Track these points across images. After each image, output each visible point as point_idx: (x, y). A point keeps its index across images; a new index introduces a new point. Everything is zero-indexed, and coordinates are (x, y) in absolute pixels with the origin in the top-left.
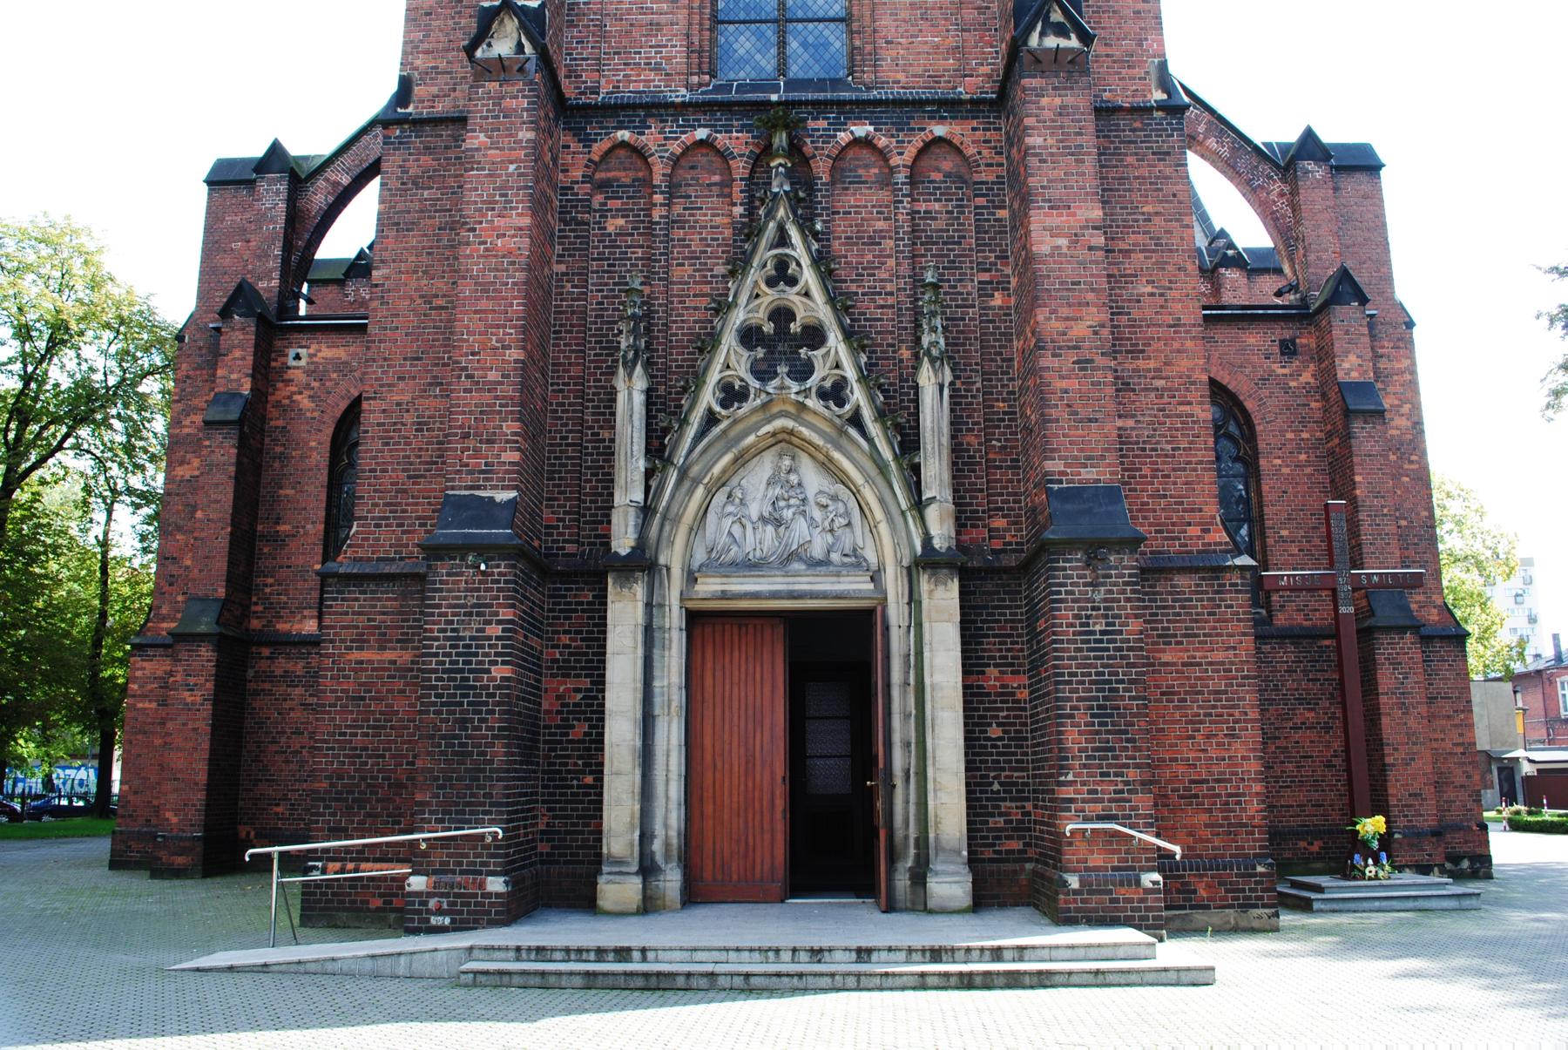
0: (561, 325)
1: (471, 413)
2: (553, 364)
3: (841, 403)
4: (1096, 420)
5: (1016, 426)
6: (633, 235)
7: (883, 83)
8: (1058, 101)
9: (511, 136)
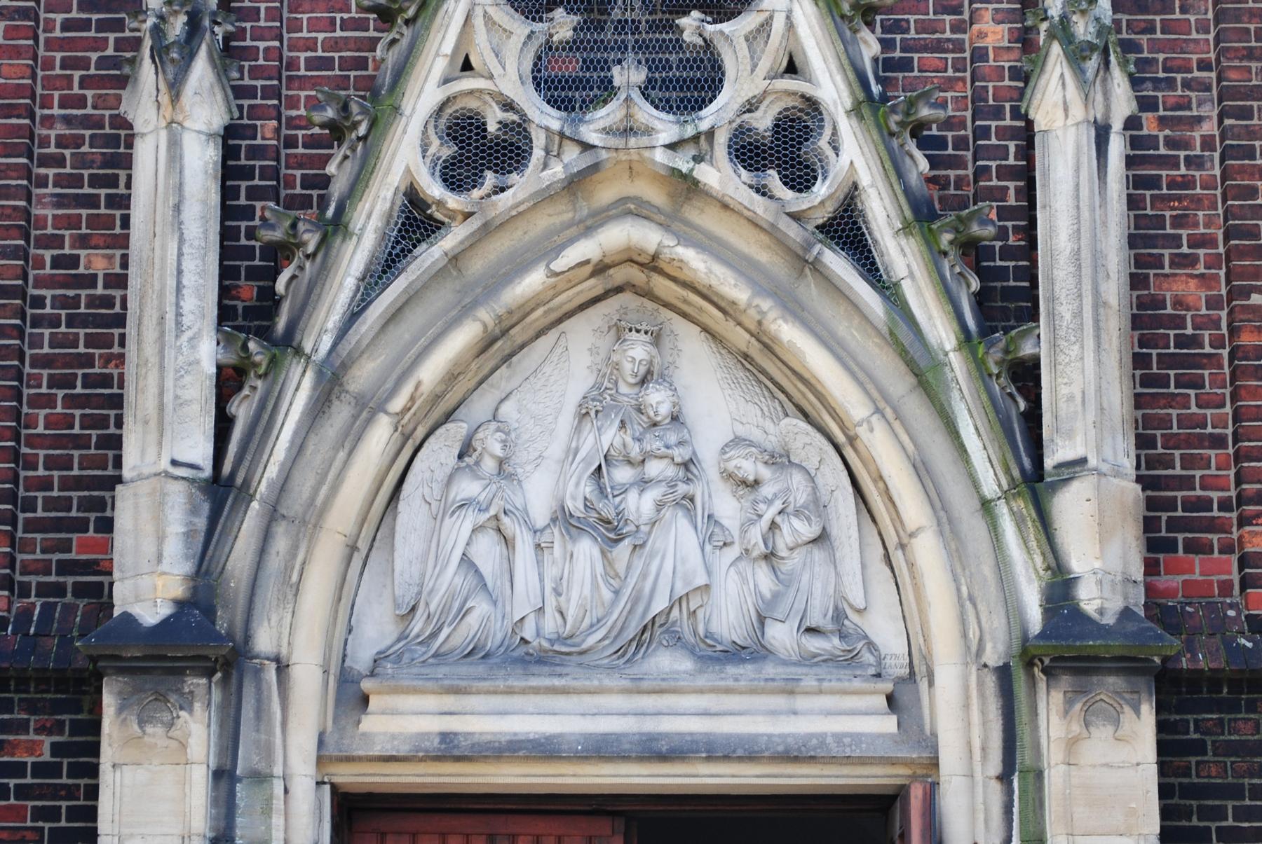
3: (801, 179)
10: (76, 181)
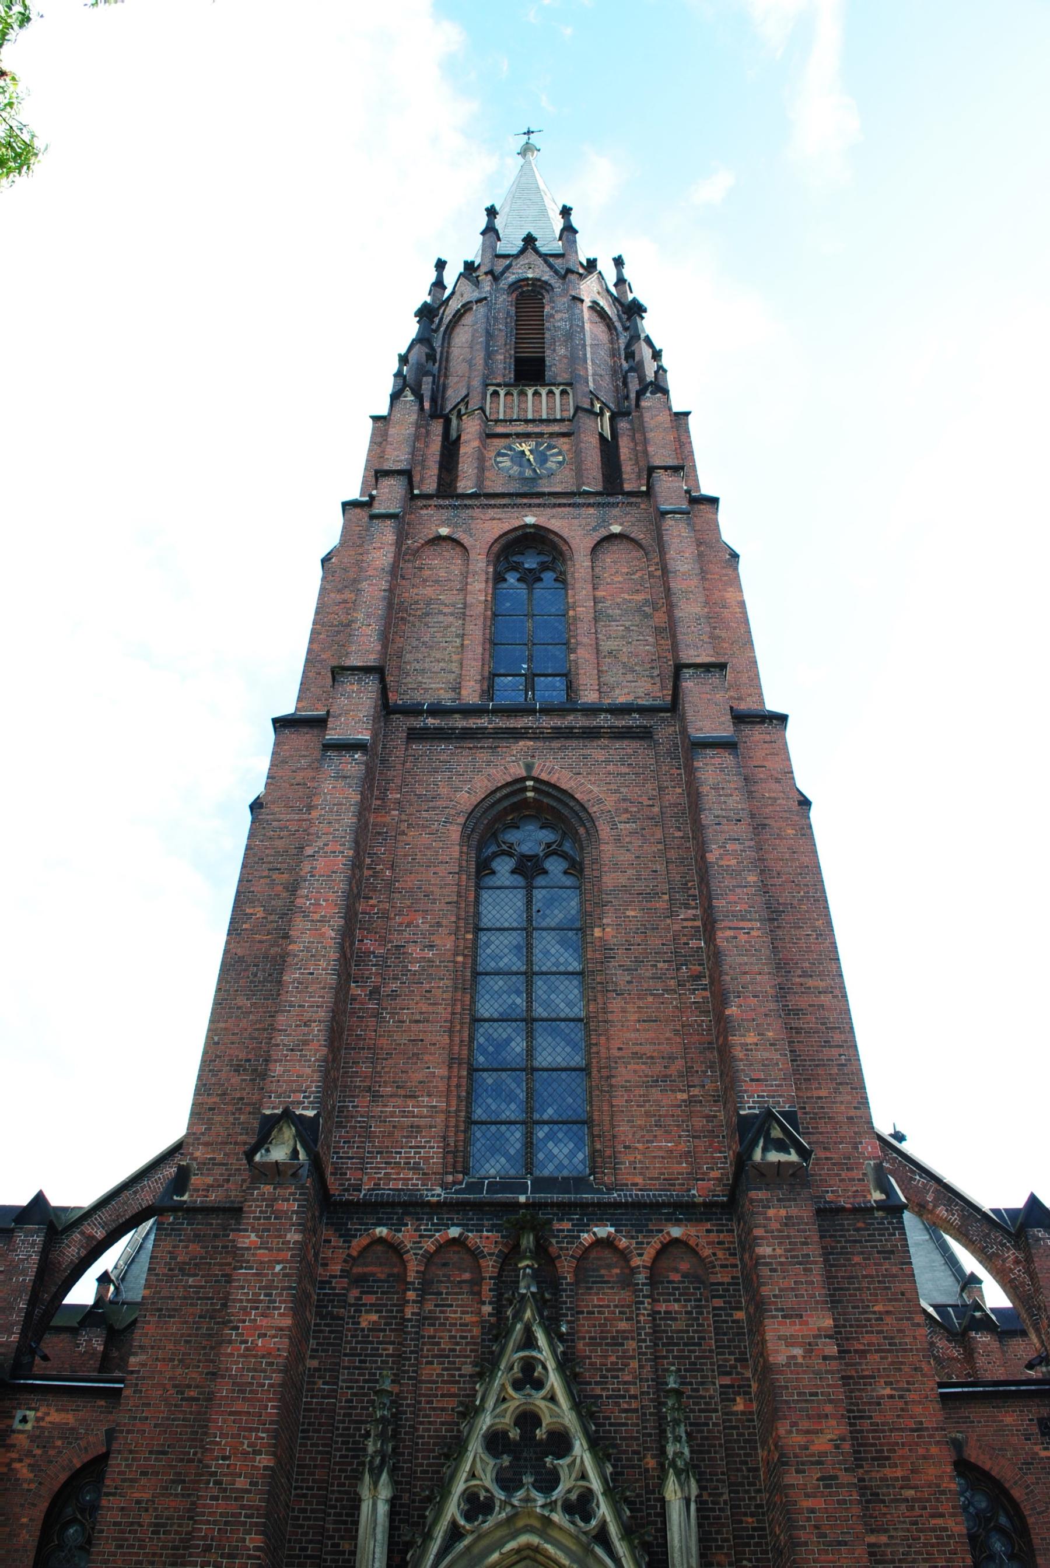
0: (309, 1424)
1: (215, 1523)
2: (299, 1466)
3: (587, 1518)
4: (845, 1543)
5: (767, 1544)
6: (385, 1330)
7: (622, 1185)
8: (783, 1212)
9: (280, 1237)
10: (340, 1515)
